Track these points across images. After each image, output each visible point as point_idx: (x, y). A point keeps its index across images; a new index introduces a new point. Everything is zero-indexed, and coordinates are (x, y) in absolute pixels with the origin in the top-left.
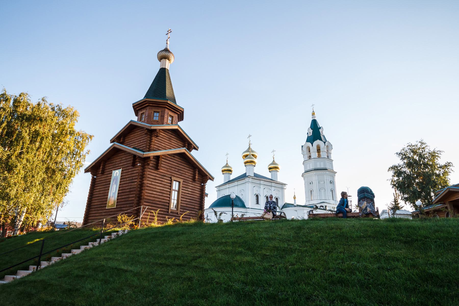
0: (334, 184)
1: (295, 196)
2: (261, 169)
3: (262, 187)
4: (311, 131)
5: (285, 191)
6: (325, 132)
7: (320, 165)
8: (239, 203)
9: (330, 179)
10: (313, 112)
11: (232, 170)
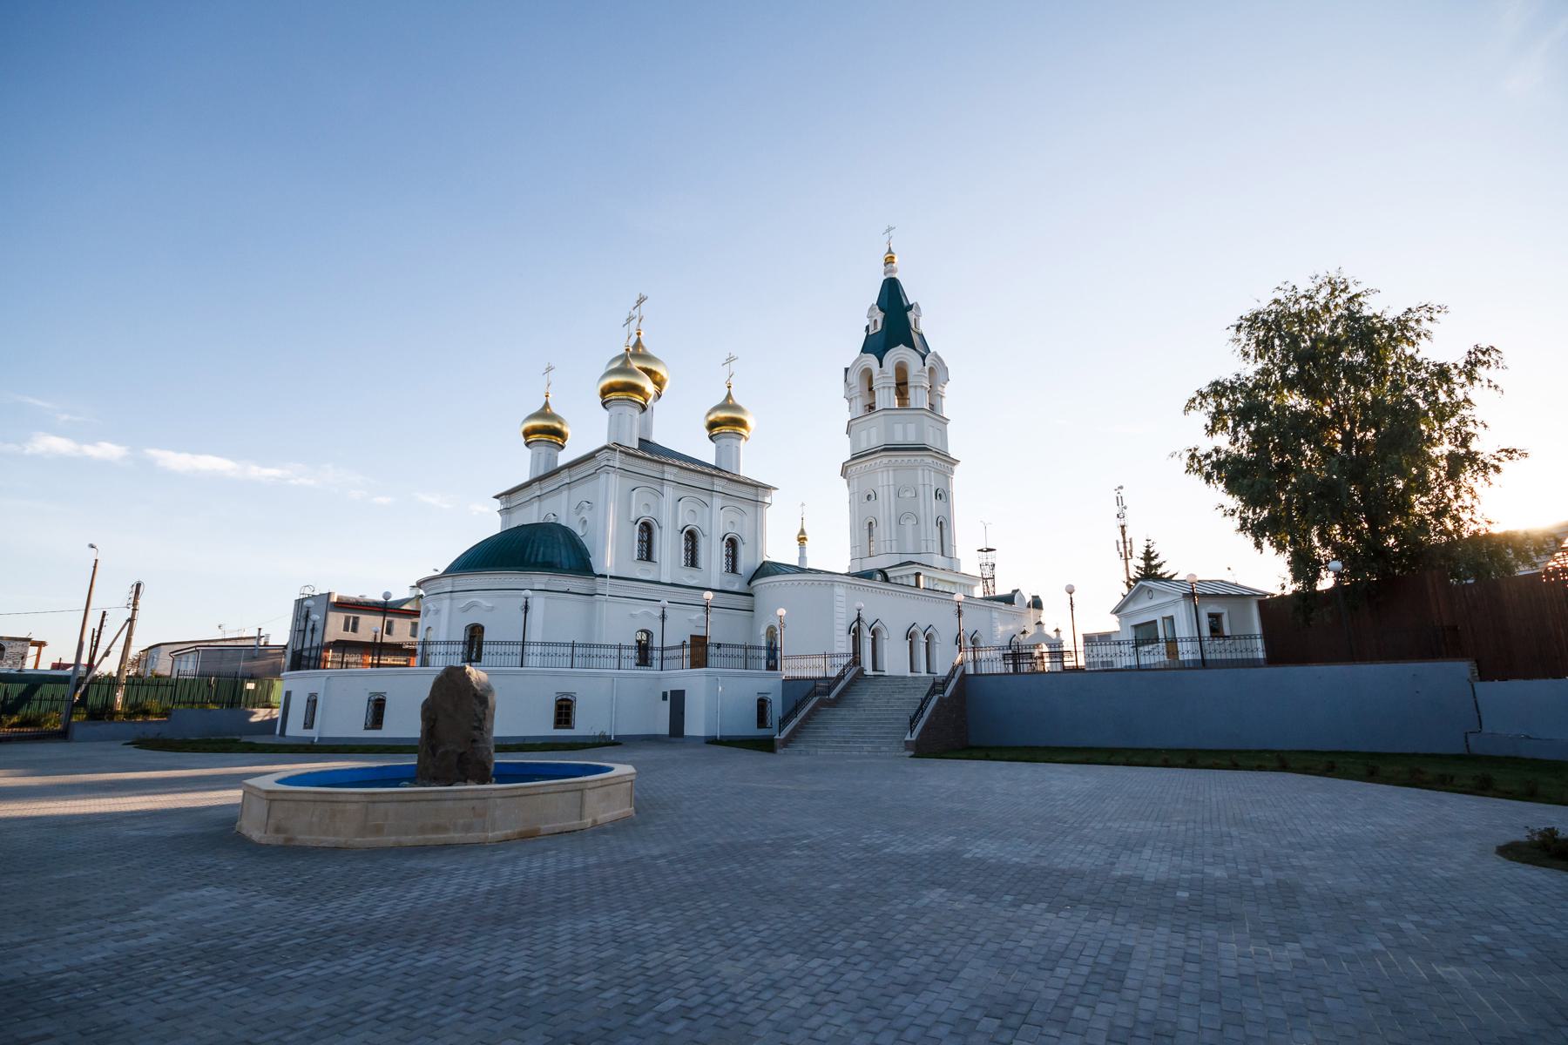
0: (947, 500)
1: (802, 532)
2: (679, 426)
3: (669, 492)
4: (879, 316)
5: (769, 513)
6: (927, 323)
7: (905, 434)
8: (563, 555)
9: (934, 481)
10: (890, 251)
11: (565, 429)
